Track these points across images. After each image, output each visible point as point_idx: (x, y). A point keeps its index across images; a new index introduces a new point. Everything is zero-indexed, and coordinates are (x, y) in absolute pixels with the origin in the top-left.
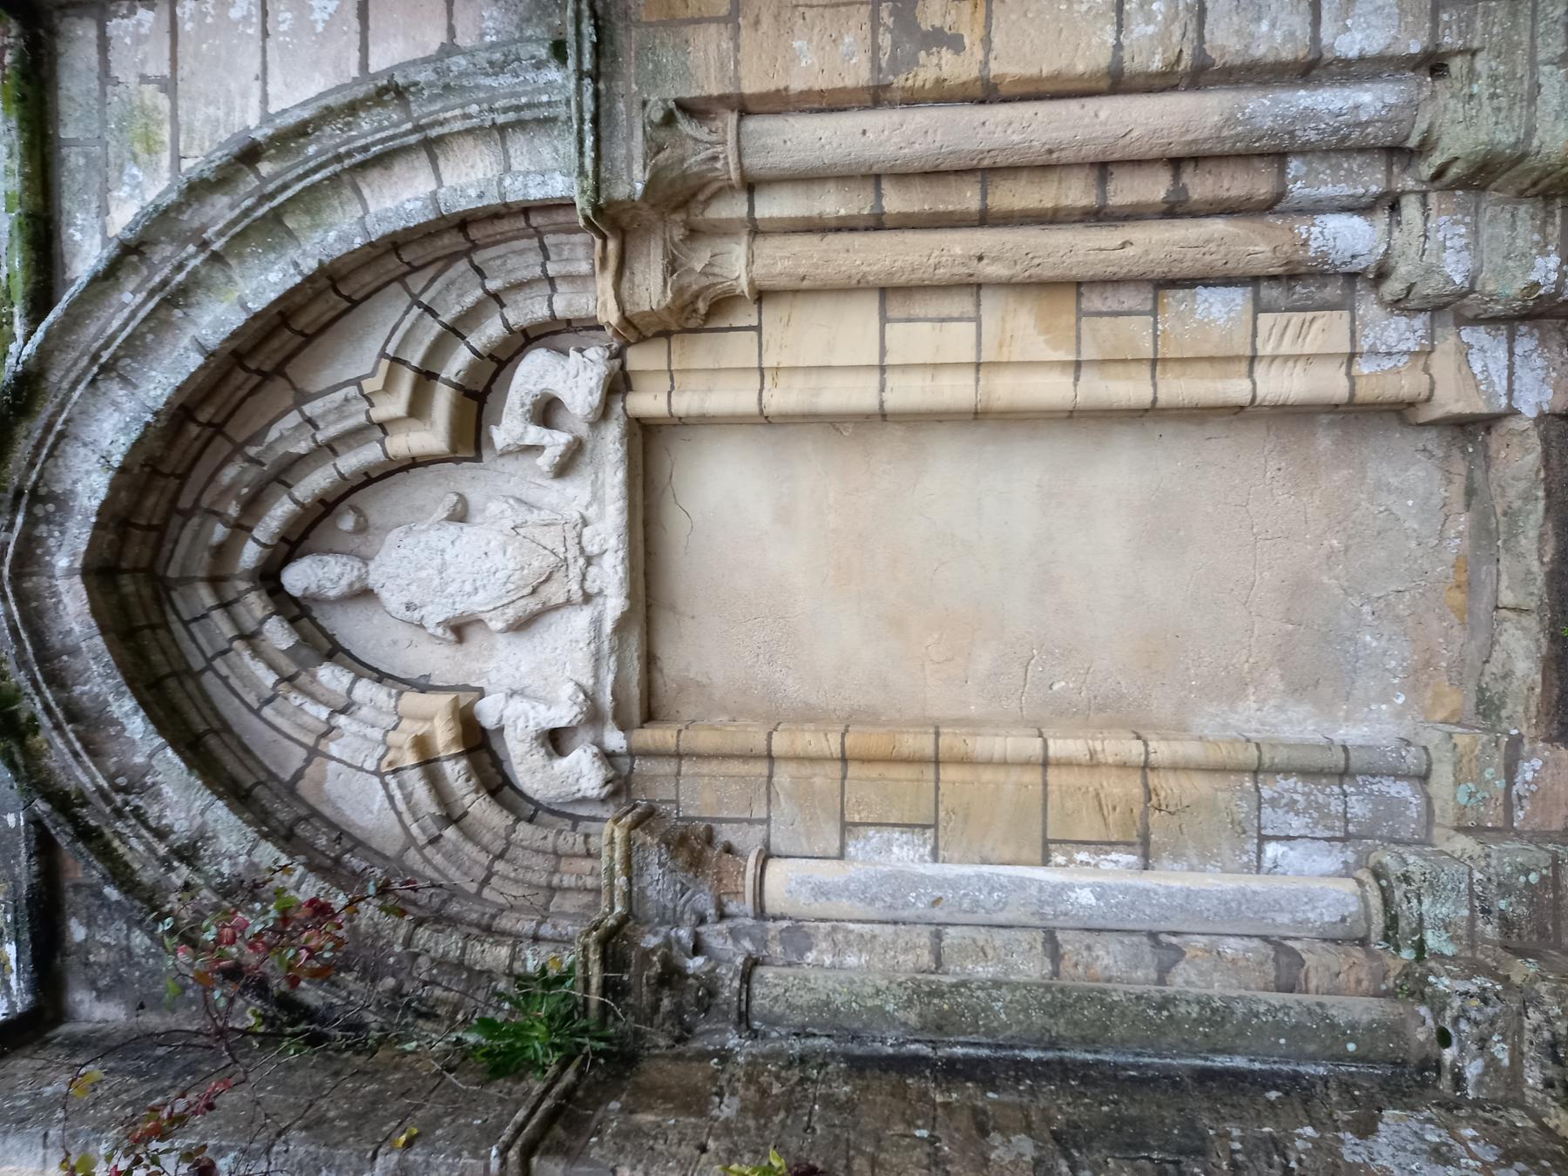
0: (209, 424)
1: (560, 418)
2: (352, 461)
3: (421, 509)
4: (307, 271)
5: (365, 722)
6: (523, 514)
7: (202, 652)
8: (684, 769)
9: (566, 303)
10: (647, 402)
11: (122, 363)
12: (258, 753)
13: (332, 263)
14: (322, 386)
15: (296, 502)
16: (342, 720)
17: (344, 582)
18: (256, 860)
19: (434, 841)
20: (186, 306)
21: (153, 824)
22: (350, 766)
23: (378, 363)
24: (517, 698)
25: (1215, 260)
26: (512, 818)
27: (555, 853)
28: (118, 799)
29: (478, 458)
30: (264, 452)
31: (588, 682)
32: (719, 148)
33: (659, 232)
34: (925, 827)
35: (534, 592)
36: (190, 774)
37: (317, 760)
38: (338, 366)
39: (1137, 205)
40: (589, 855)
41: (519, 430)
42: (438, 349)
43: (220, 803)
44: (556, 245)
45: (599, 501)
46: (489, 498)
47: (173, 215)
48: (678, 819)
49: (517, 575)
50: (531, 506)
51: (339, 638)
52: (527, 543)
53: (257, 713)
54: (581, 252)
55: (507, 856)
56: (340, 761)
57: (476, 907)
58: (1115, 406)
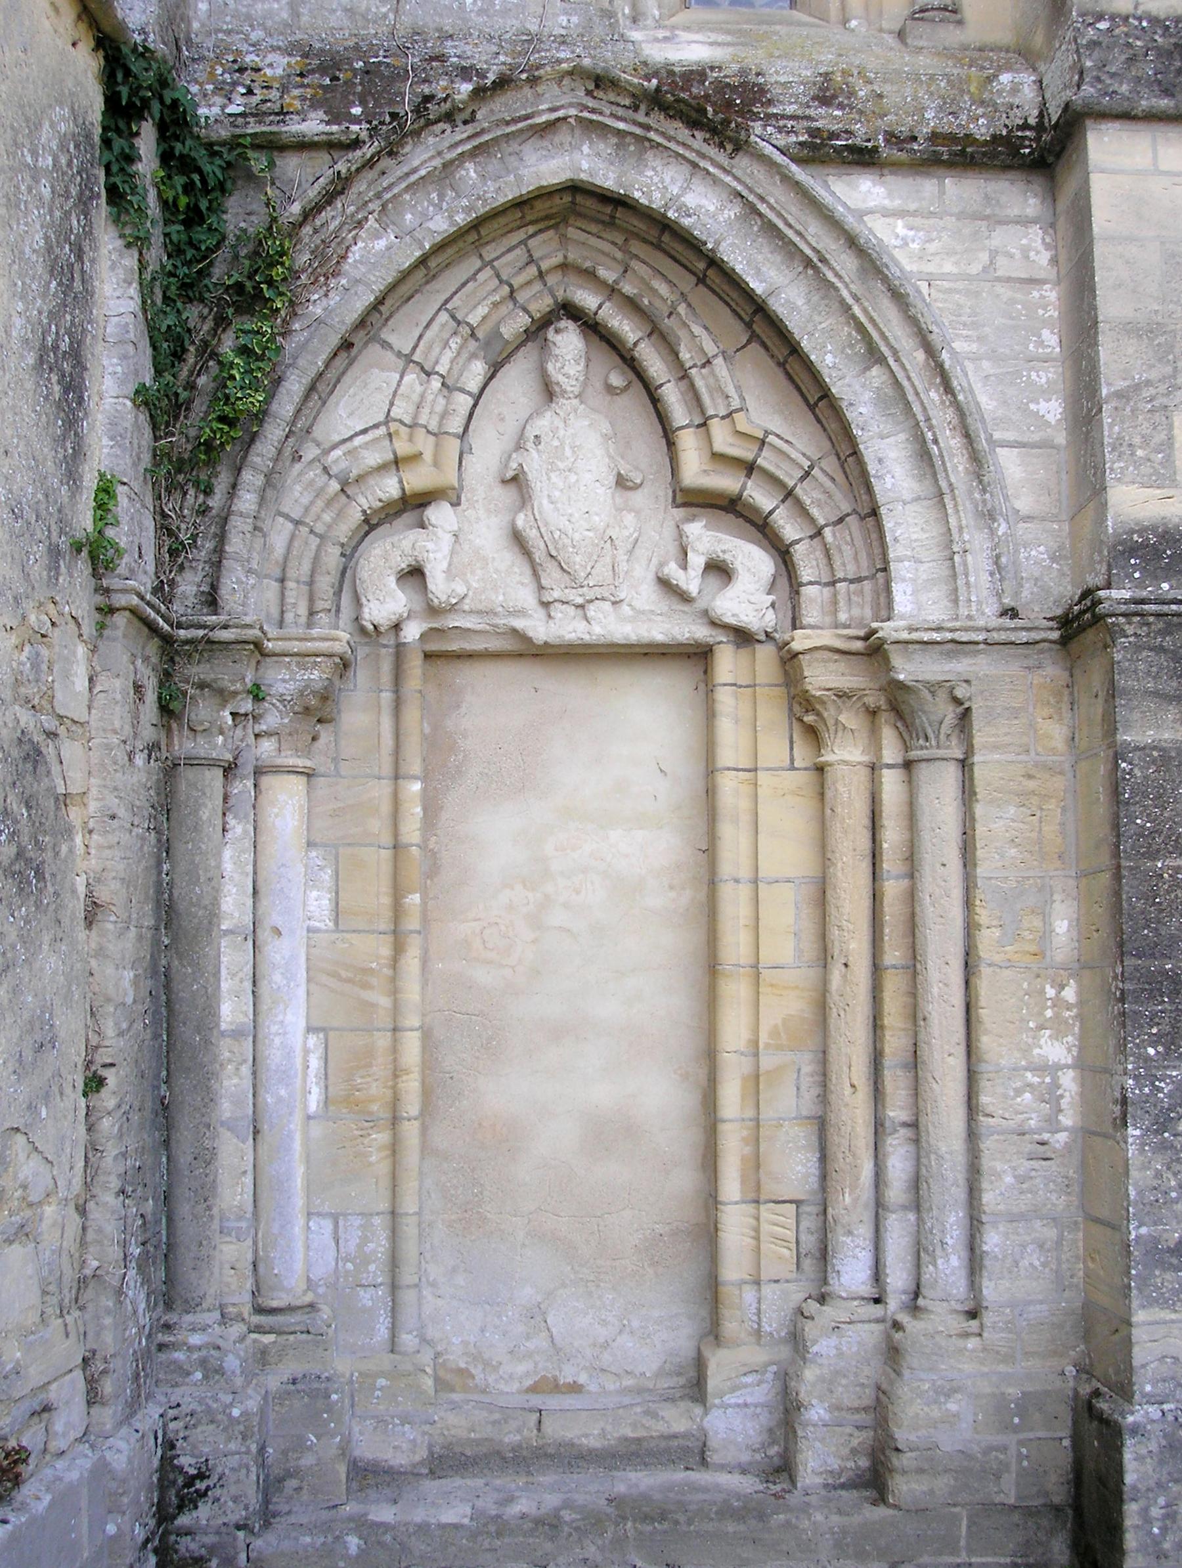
0: (705, 275)
1: (714, 581)
2: (672, 394)
6: (623, 547)
7: (497, 258)
17: (561, 379)
25: (840, 1161)
28: (375, 206)
32: (934, 743)
33: (871, 685)
34: (336, 923)
37: (401, 363)
39: (883, 1094)
40: (312, 613)
44: (862, 592)
49: (567, 541)
51: (507, 366)
56: (400, 381)
58: (719, 1087)
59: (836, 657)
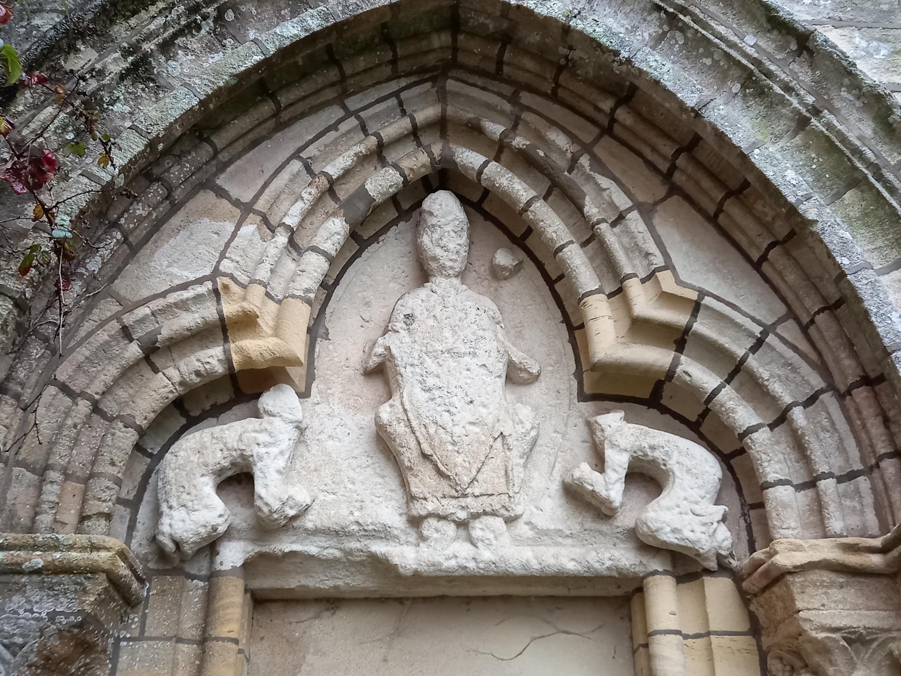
0: (613, 120)
1: (638, 495)
3: (519, 336)
4: (802, 208)
5: (278, 262)
6: (518, 447)
8: (184, 647)
9: (786, 503)
10: (665, 603)
11: (678, 34)
12: (250, 155)
13: (813, 234)
14: (660, 230)
15: (529, 203)
16: (282, 239)
17: (438, 252)
18: (124, 135)
19: (126, 333)
20: (745, 95)
21: (179, 41)
22: (227, 245)
23: (693, 288)
24: (295, 434)
26: (144, 423)
27: (92, 476)
29: (583, 397)
30: (584, 174)
31: (310, 521)
35: (425, 456)
36: (233, 76)
37: (237, 212)
38: (685, 247)
41: (623, 443)
42: (713, 353)
43: (195, 102)
44: (857, 491)
45: (536, 539)
46: (536, 409)
47: (846, 81)
48: (118, 640)
50: (528, 455)
52: (484, 450)
53: (296, 155)
54: (854, 521)
55: (95, 417)
56: (234, 235)
57: (34, 378)
59: (841, 579)
